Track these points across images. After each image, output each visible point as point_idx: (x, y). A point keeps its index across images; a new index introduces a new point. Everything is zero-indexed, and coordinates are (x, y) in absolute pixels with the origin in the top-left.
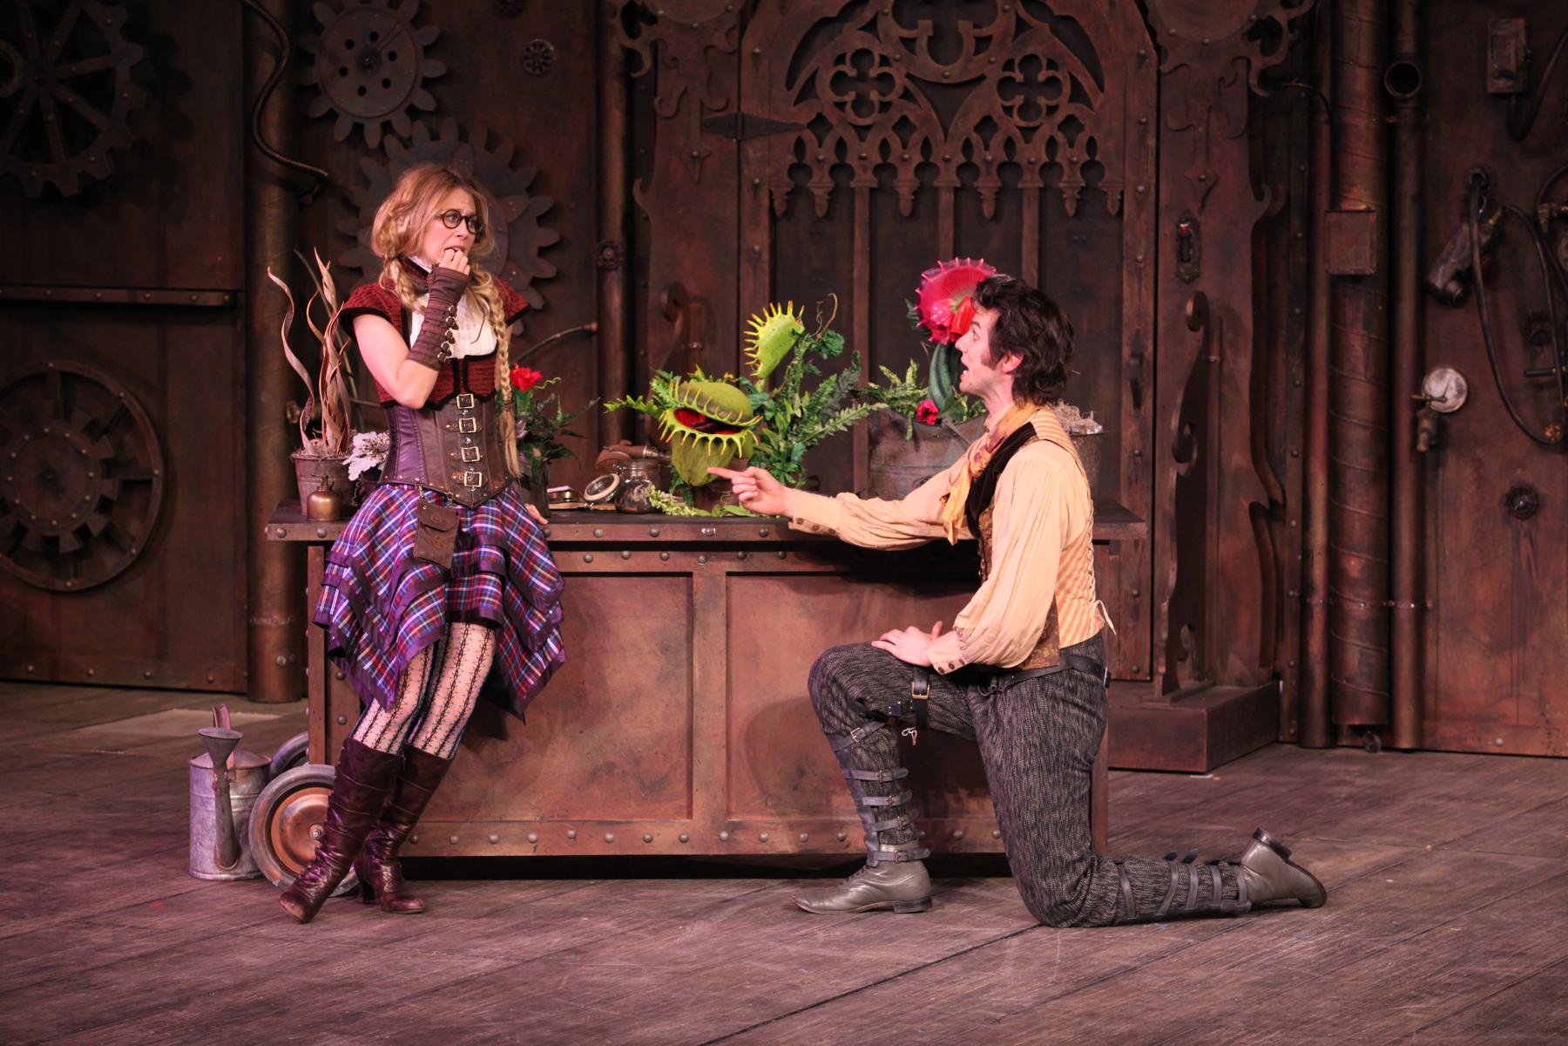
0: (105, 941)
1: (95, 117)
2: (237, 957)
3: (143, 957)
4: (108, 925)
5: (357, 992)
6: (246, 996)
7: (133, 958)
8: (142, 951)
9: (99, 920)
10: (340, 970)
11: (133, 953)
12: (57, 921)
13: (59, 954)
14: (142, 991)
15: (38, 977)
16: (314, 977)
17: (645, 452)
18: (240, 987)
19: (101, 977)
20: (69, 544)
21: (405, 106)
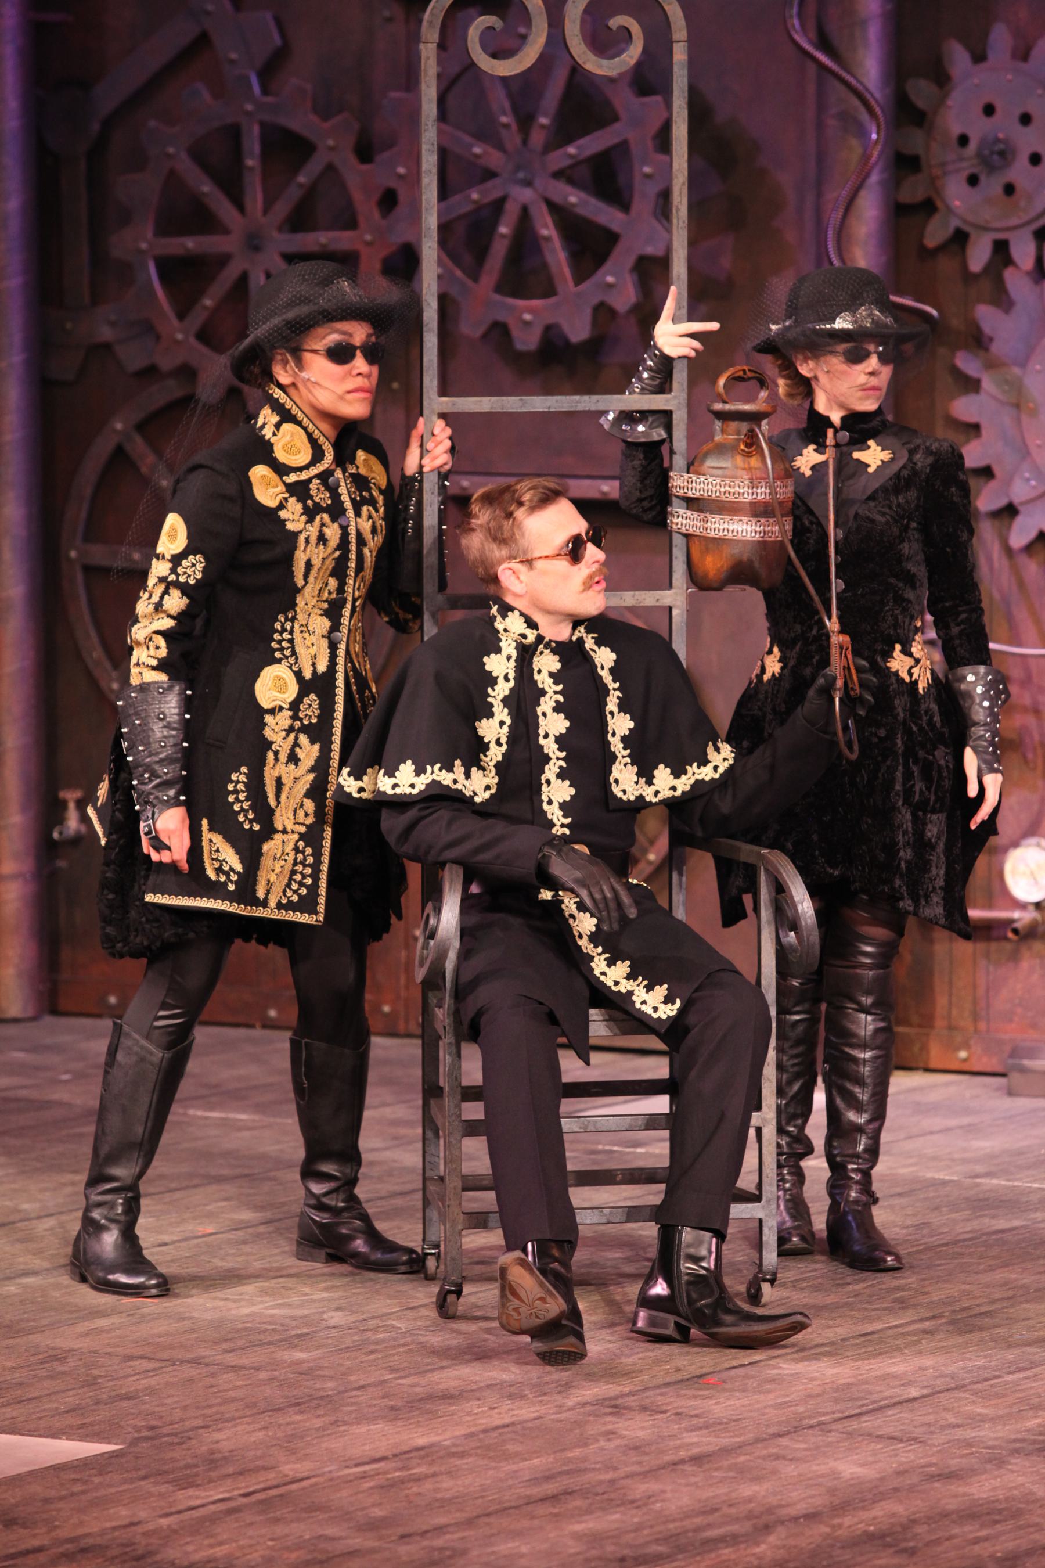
0: (641, 1434)
1: (607, 216)
2: (832, 1464)
3: (697, 1460)
4: (644, 1409)
5: (1009, 1525)
6: (853, 1523)
7: (682, 1462)
8: (695, 1451)
9: (631, 1401)
10: (983, 1488)
11: (683, 1454)
12: (570, 1403)
13: (577, 1452)
14: (704, 1513)
15: (550, 1488)
16: (951, 1496)
17: (330, 1385)
18: (842, 1507)
19: (640, 1489)
20: (935, 233)
21: (1001, 236)
